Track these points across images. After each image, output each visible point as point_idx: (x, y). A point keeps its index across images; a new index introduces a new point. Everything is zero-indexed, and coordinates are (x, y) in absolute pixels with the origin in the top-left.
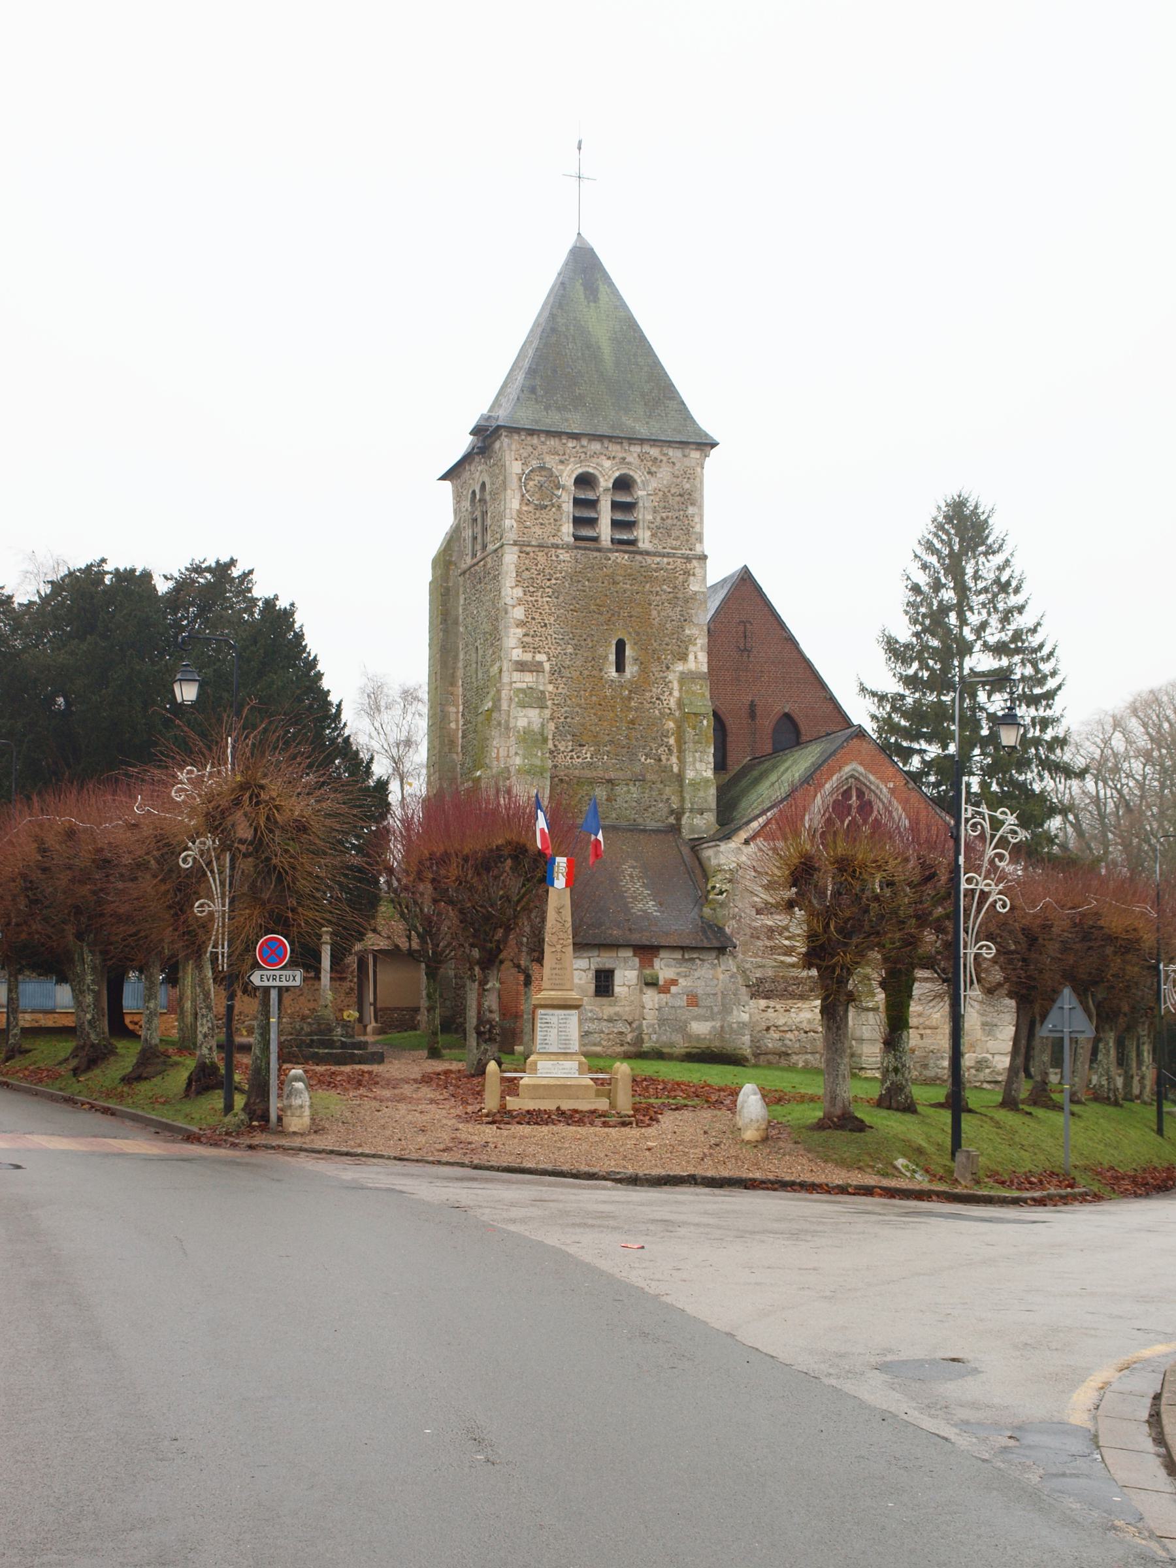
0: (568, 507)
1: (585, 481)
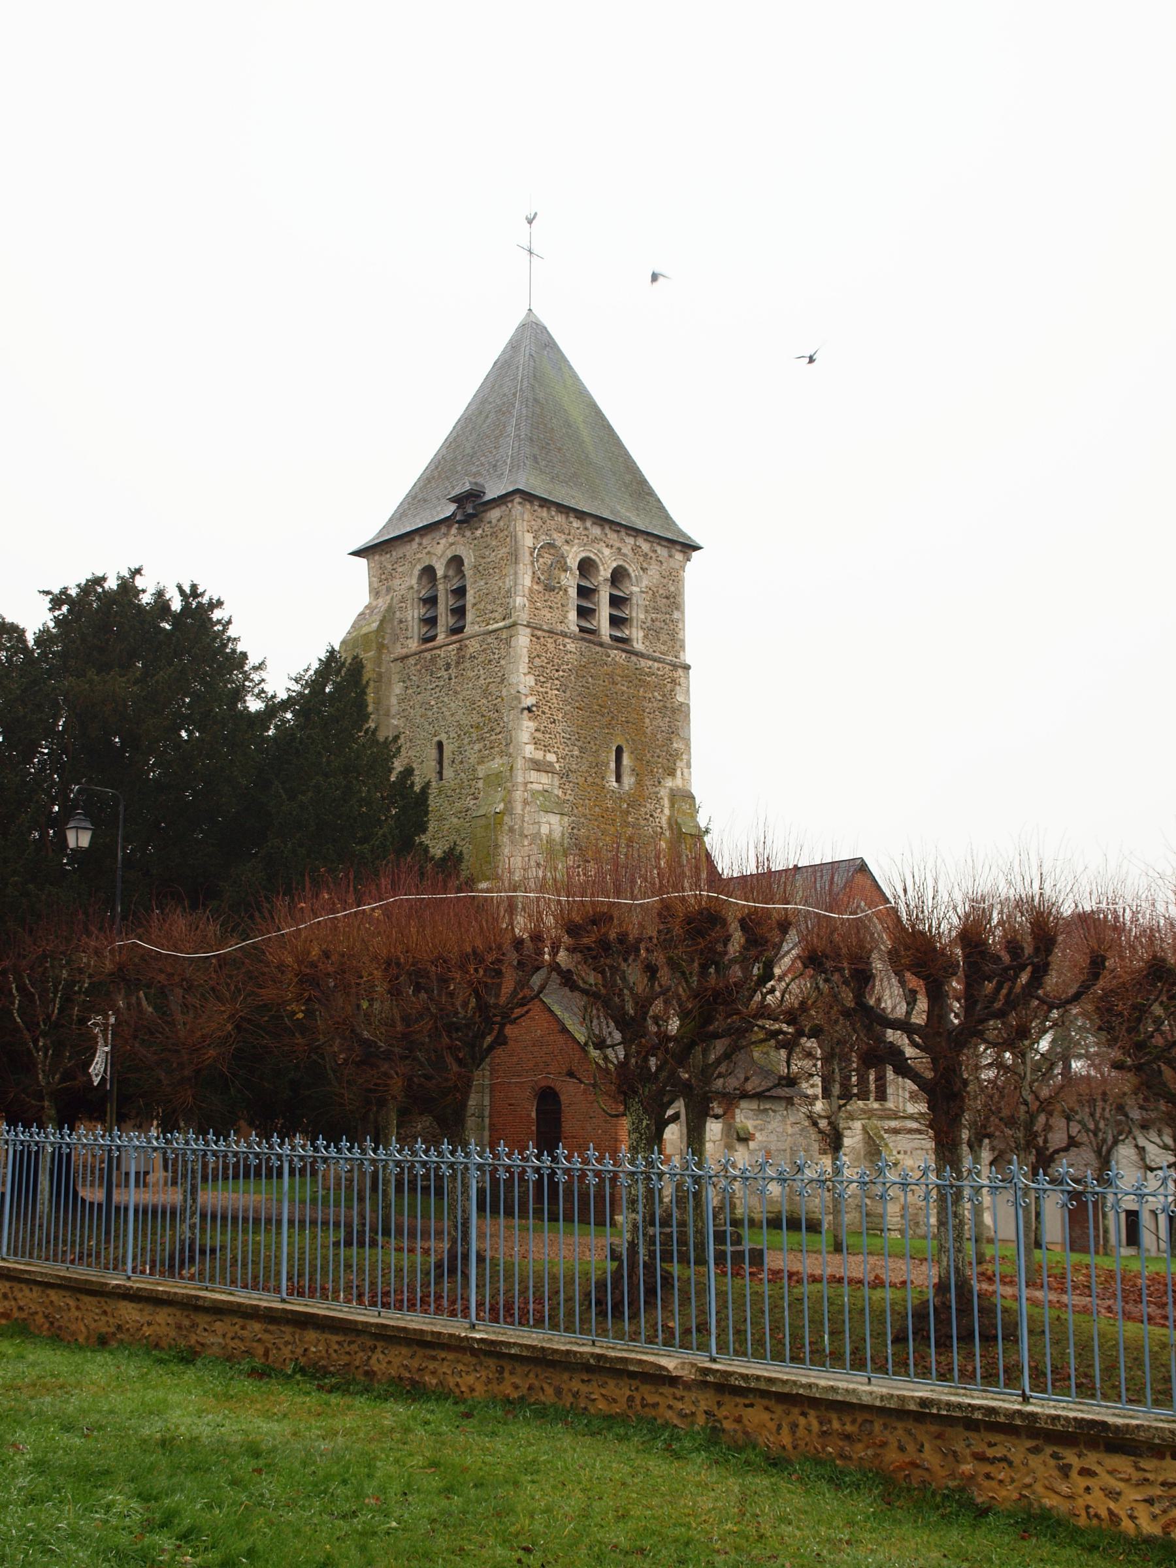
0: (573, 592)
1: (586, 567)
